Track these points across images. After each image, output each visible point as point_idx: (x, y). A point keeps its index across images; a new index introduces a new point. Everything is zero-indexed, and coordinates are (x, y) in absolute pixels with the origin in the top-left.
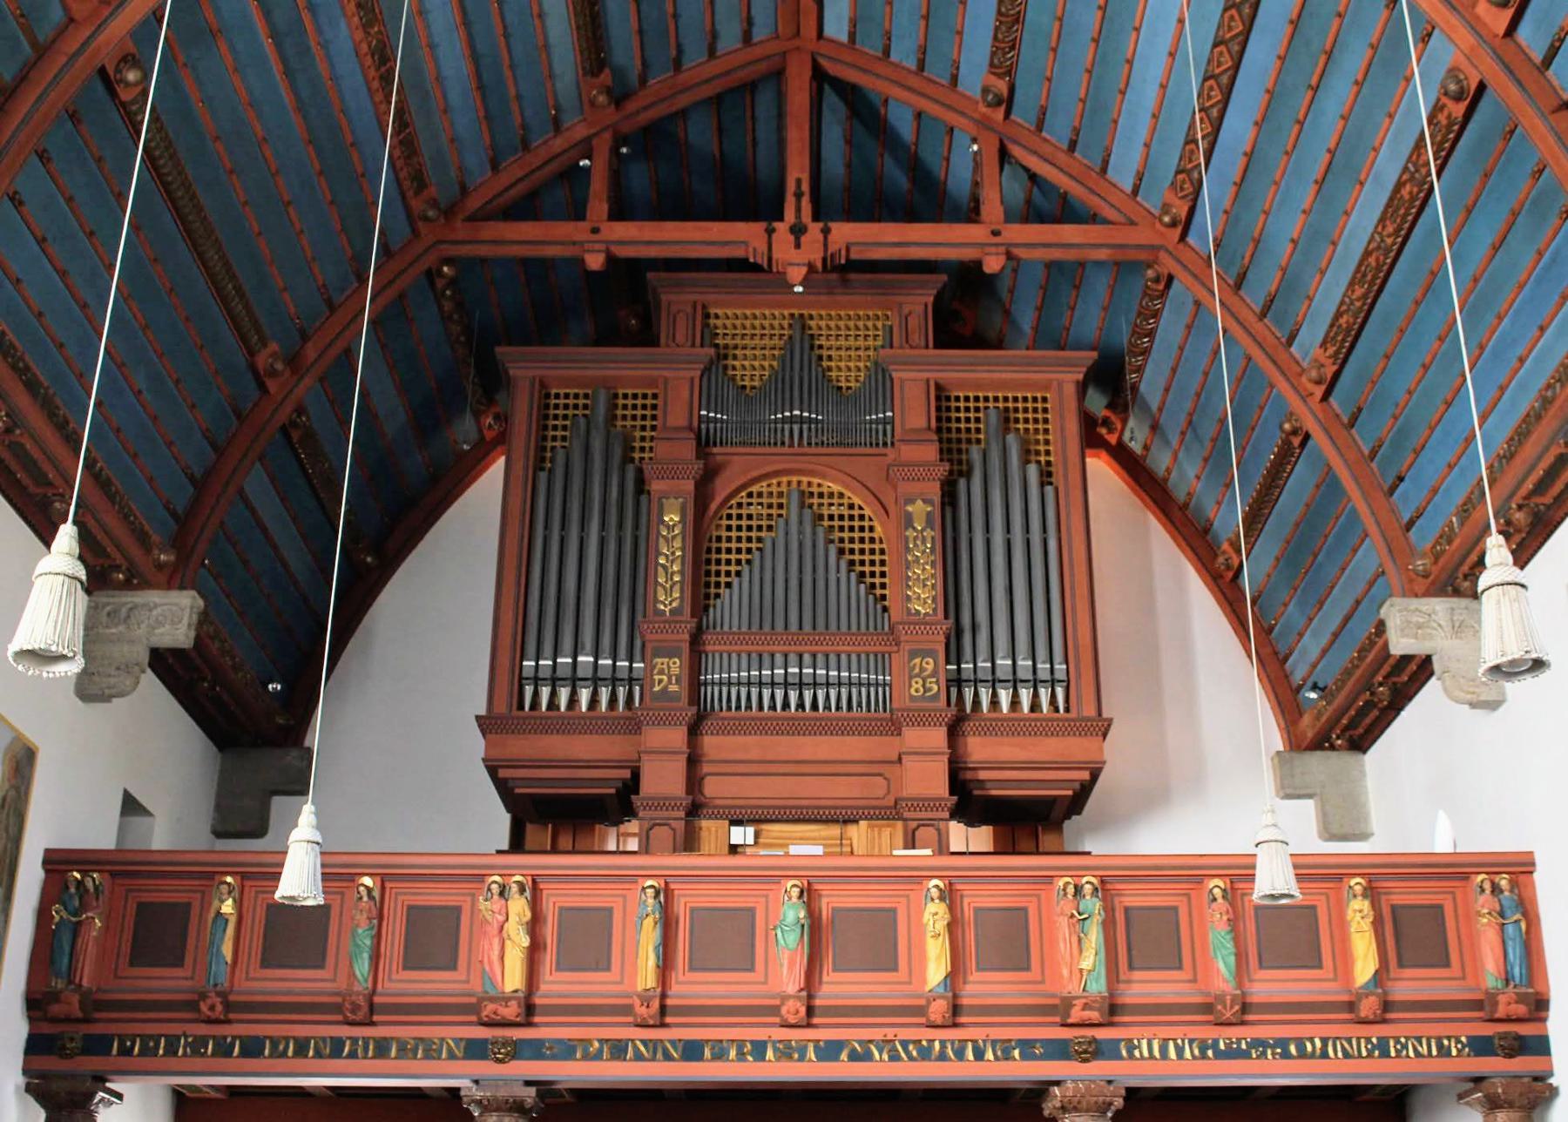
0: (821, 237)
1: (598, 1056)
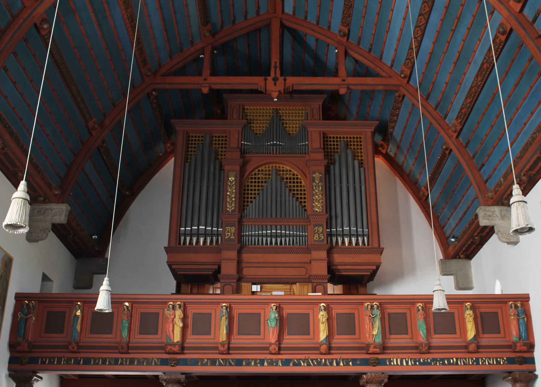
0: (283, 82)
1: (206, 364)
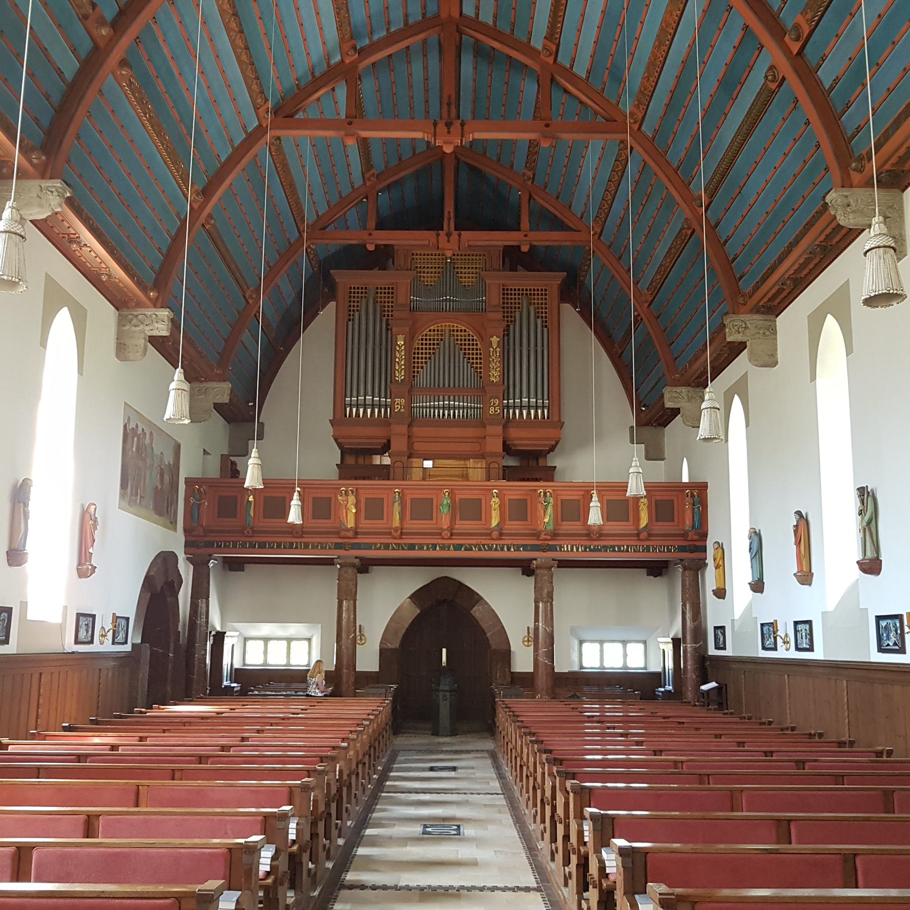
0: (457, 237)
1: (380, 549)
